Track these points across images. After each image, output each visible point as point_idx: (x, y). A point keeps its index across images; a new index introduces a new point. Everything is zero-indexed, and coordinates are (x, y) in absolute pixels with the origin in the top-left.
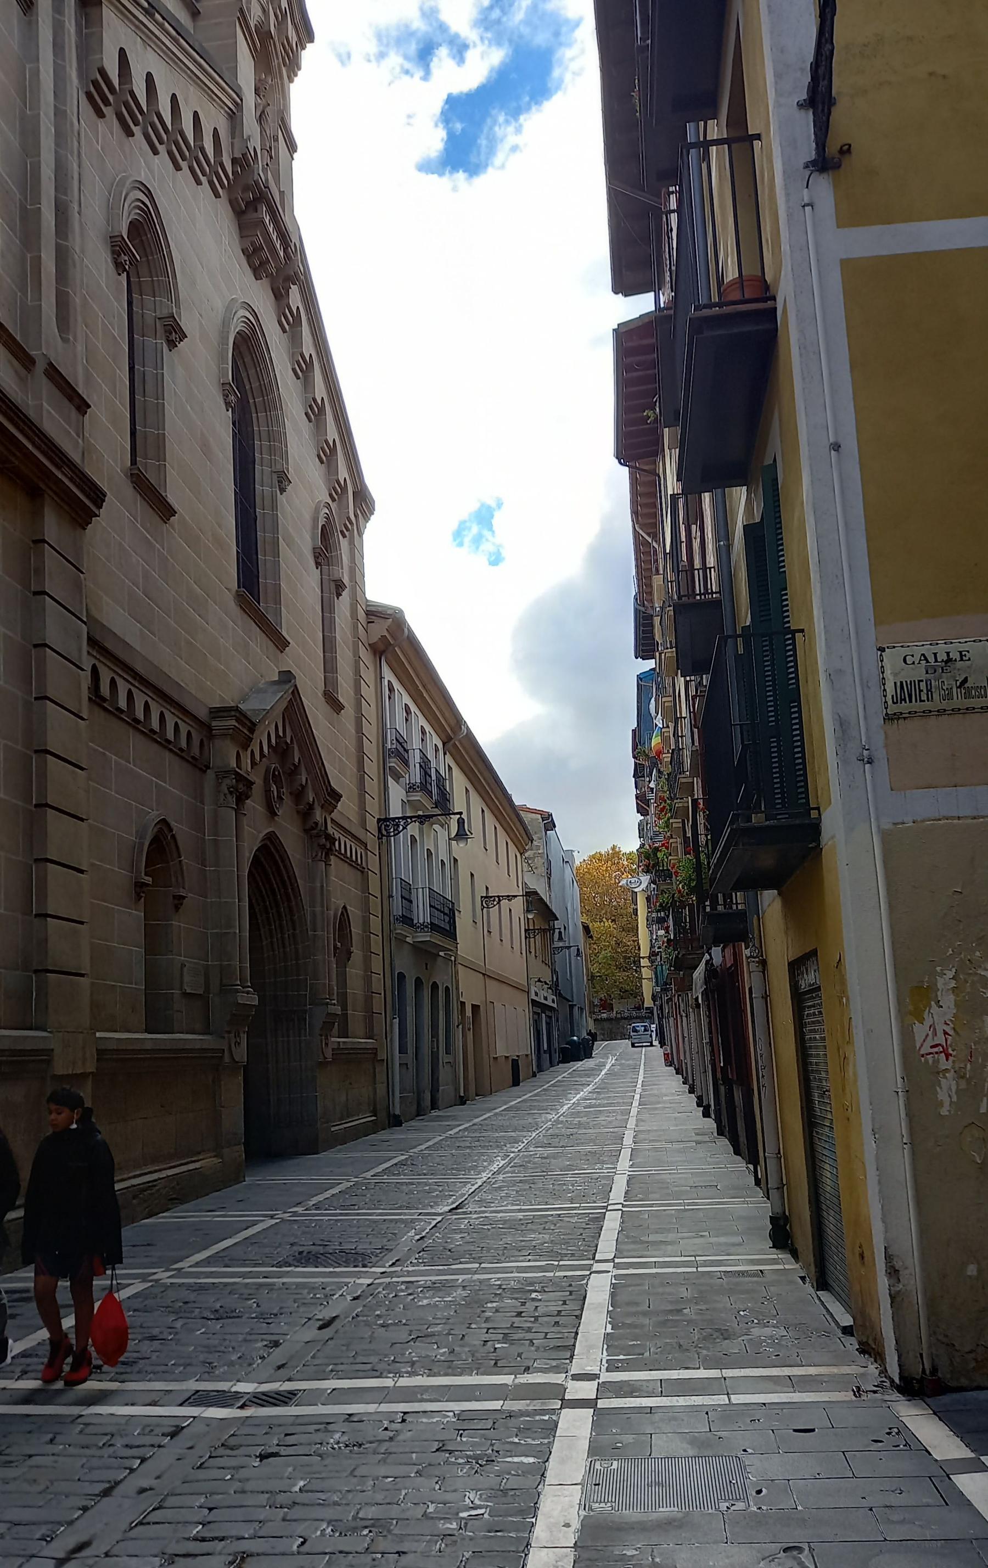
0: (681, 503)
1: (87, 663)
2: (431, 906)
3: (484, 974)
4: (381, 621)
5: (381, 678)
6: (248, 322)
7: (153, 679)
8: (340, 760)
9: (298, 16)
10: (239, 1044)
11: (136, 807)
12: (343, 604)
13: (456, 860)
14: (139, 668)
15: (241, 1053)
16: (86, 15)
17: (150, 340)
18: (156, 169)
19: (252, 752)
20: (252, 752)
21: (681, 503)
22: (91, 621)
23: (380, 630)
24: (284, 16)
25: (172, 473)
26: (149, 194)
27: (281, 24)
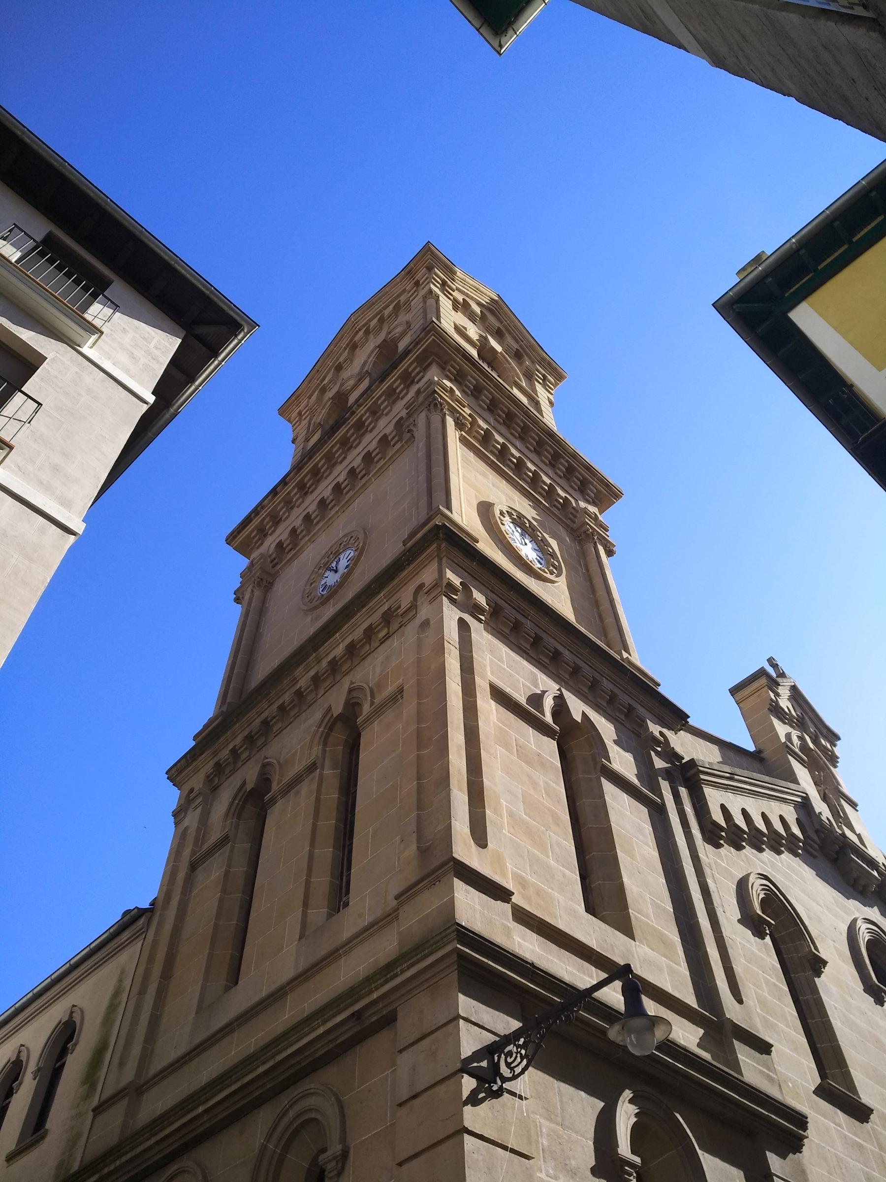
6: (871, 931)
9: (825, 731)
26: (766, 878)
27: (815, 741)
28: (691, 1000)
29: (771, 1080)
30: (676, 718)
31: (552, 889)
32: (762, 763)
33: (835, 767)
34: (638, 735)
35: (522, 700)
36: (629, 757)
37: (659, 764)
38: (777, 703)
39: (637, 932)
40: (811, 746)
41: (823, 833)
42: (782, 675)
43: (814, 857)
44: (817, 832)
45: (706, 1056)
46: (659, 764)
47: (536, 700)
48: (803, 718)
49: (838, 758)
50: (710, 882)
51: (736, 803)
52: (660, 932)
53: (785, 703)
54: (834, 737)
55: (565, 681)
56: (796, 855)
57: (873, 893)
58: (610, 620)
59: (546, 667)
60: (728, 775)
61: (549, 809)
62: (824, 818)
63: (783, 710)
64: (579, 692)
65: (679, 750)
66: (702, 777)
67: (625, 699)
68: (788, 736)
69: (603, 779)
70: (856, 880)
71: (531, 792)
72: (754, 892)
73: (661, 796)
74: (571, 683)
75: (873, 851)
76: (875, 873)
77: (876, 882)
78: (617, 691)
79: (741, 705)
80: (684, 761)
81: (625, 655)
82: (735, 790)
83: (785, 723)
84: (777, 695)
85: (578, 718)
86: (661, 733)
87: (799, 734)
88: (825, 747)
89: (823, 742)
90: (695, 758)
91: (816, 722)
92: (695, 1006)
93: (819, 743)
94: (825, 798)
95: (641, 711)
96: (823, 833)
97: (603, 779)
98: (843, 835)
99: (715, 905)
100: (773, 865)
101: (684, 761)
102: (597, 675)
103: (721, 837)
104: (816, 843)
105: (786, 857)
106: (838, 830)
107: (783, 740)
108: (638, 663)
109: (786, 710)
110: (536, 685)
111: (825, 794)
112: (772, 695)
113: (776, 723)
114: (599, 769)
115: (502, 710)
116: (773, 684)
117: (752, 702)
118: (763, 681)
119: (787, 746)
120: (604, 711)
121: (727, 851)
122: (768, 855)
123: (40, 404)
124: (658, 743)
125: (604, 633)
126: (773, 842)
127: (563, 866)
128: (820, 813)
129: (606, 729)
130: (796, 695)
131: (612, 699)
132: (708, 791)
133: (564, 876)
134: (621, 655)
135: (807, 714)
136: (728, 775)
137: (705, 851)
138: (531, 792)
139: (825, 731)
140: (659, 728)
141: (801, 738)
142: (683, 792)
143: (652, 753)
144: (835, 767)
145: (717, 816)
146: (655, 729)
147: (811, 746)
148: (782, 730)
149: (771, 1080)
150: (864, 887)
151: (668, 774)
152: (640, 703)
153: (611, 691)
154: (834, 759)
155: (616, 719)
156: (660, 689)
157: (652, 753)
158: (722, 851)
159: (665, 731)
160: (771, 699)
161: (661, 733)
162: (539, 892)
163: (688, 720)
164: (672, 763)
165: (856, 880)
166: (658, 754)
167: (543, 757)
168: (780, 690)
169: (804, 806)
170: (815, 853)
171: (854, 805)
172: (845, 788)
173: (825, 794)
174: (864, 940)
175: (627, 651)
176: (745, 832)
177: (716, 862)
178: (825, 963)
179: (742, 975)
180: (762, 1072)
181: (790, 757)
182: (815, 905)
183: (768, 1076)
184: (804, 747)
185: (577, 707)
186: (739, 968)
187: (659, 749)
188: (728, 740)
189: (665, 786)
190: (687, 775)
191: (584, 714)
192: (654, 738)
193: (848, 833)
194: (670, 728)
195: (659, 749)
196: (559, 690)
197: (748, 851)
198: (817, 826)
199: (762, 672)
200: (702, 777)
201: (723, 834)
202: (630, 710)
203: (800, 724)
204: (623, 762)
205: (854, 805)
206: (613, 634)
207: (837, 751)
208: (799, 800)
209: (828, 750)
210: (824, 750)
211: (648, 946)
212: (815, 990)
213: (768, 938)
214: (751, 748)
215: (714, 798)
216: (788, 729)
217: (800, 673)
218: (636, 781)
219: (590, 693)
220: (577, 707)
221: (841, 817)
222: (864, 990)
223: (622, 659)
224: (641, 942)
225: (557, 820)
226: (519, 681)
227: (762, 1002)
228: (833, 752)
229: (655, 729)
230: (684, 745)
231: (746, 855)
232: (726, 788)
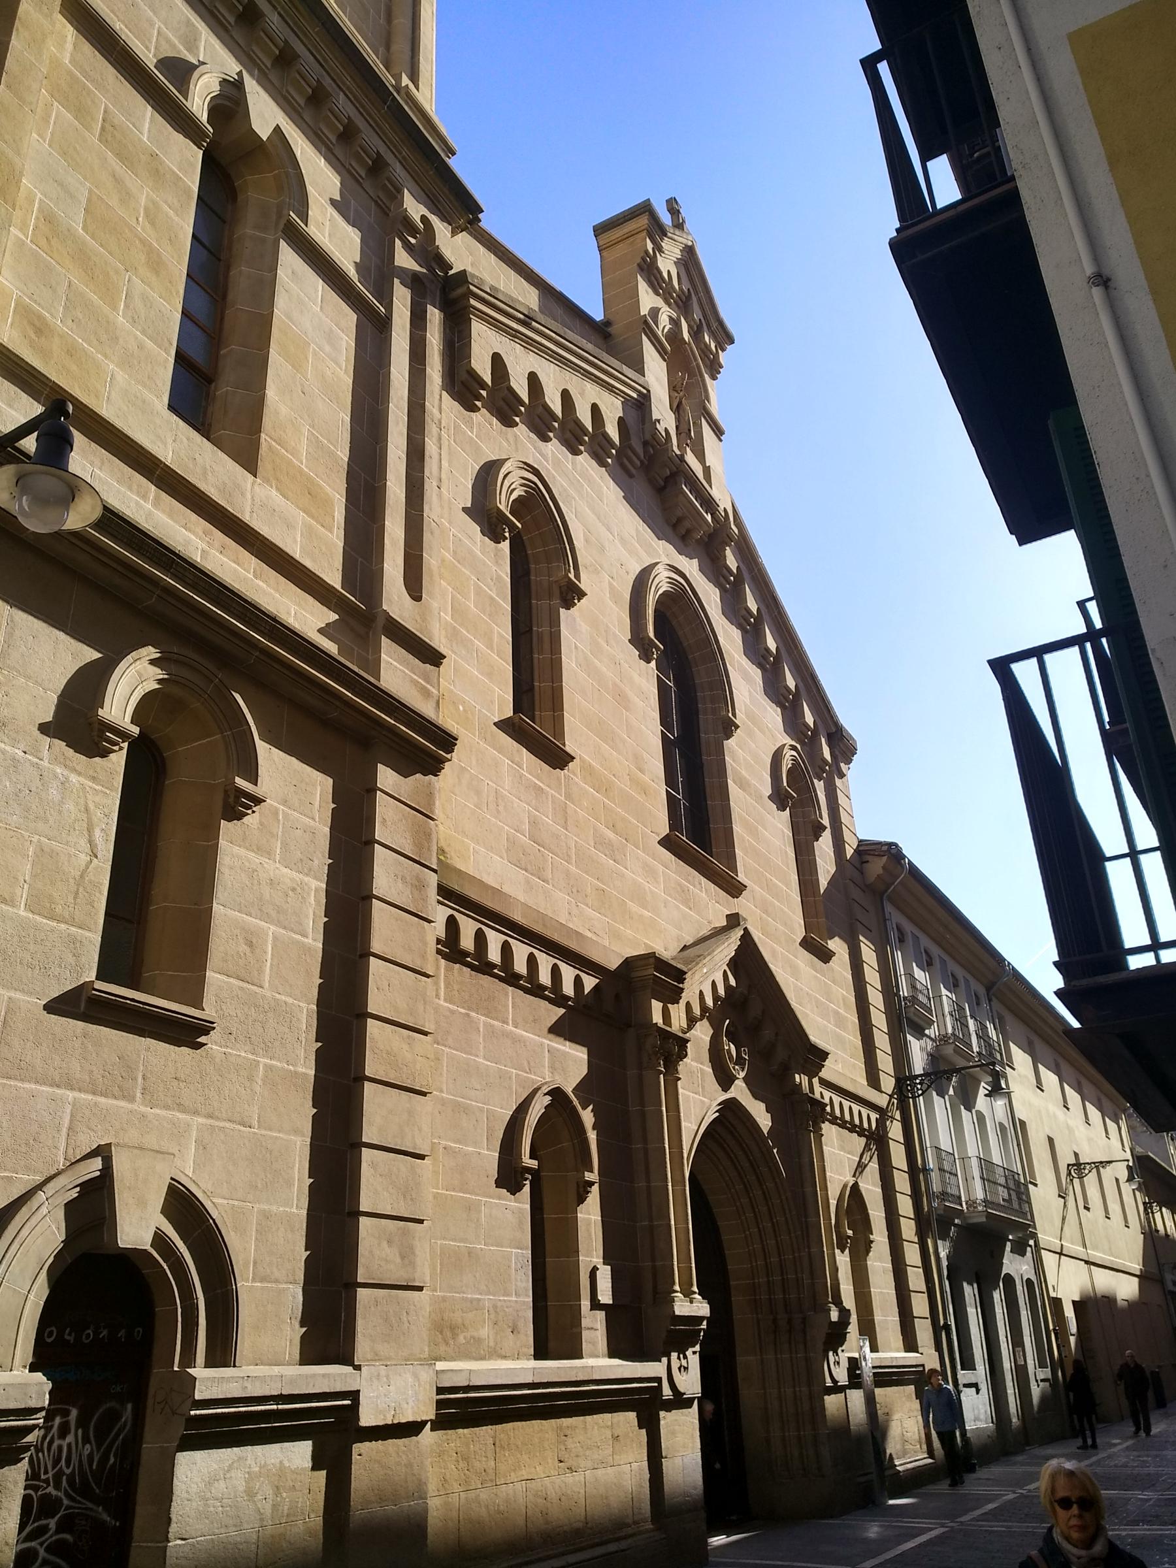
0: (883, 68)
1: (441, 914)
2: (956, 1175)
3: (1087, 1262)
4: (876, 859)
5: (885, 920)
6: (672, 581)
7: (538, 928)
8: (837, 1013)
9: (715, 325)
10: (686, 1369)
11: (517, 1075)
12: (824, 846)
13: (1023, 1123)
14: (517, 917)
15: (690, 1382)
16: (459, 332)
17: (544, 603)
18: (551, 456)
19: (688, 1005)
20: (688, 1005)
21: (883, 68)
22: (443, 868)
23: (876, 867)
24: (700, 327)
25: (571, 720)
26: (536, 472)
27: (696, 333)
28: (334, 579)
29: (426, 694)
30: (462, 208)
31: (106, 356)
32: (608, 339)
33: (714, 378)
34: (384, 211)
35: (149, 59)
36: (353, 236)
37: (403, 259)
38: (654, 259)
39: (264, 464)
40: (686, 336)
41: (653, 447)
42: (679, 225)
43: (631, 476)
44: (645, 444)
45: (331, 647)
46: (403, 259)
47: (181, 71)
48: (689, 297)
49: (721, 367)
50: (431, 446)
51: (521, 364)
52: (309, 478)
53: (667, 265)
54: (725, 338)
55: (260, 69)
56: (602, 463)
57: (697, 541)
58: (401, 21)
59: (226, 30)
60: (522, 316)
61: (143, 242)
62: (661, 428)
63: (660, 273)
64: (285, 98)
65: (447, 253)
66: (472, 302)
67: (372, 140)
68: (655, 312)
69: (283, 244)
70: (679, 520)
71: (114, 202)
72: (507, 483)
73: (389, 307)
74: (272, 77)
75: (716, 492)
76: (709, 518)
77: (706, 528)
78: (360, 122)
79: (605, 253)
80: (451, 272)
81: (405, 81)
82: (529, 343)
83: (658, 294)
84: (659, 248)
85: (264, 133)
86: (424, 219)
87: (674, 315)
88: (708, 347)
89: (707, 338)
90: (469, 269)
91: (707, 308)
92: (338, 586)
93: (700, 340)
94: (677, 409)
95: (398, 171)
96: (653, 447)
97: (283, 244)
98: (681, 458)
99: (427, 473)
100: (557, 463)
101: (451, 272)
102: (327, 82)
103: (479, 397)
104: (638, 458)
105: (585, 460)
106: (675, 449)
107: (644, 311)
108: (430, 108)
109: (665, 275)
110: (192, 45)
111: (680, 404)
112: (650, 246)
113: (643, 287)
114: (281, 226)
115: (87, 48)
116: (657, 231)
117: (621, 250)
118: (643, 221)
119: (646, 322)
120: (329, 149)
121: (483, 418)
122: (554, 448)
123: (1002, 667)
124: (414, 231)
125: (386, 43)
126: (568, 435)
127: (143, 332)
128: (659, 421)
129: (321, 177)
130: (689, 260)
131: (348, 135)
132: (479, 330)
133: (141, 347)
134: (398, 78)
135: (697, 293)
136: (522, 316)
137: (442, 407)
138: (114, 202)
139: (715, 325)
140: (424, 211)
141: (675, 322)
142: (434, 315)
143: (398, 243)
144: (714, 378)
145: (482, 366)
146: (415, 209)
147: (686, 336)
148: (648, 300)
149: (426, 694)
150: (688, 532)
151: (414, 282)
152: (400, 160)
153: (349, 118)
154: (714, 368)
155: (349, 172)
156: (453, 162)
157: (398, 243)
158: (475, 416)
159: (434, 220)
160: (647, 252)
161: (424, 219)
162: (72, 351)
163: (480, 216)
164: (431, 269)
165: (679, 520)
166: (408, 247)
167: (162, 163)
168: (666, 244)
169: (640, 405)
170: (633, 471)
171: (718, 432)
172: (714, 407)
173: (680, 404)
174: (657, 590)
175: (414, 77)
176: (522, 403)
177: (456, 427)
178: (581, 594)
179: (435, 569)
180: (416, 683)
181: (644, 337)
182: (603, 530)
183: (424, 688)
184: (674, 335)
185: (265, 114)
186: (431, 560)
187: (413, 241)
188: (559, 286)
189: (402, 297)
190: (450, 294)
191: (277, 129)
192: (407, 222)
193: (690, 458)
194: (444, 218)
195: (413, 241)
196: (240, 74)
197: (521, 431)
198: (648, 437)
199: (645, 209)
200: (472, 302)
201: (484, 393)
202: (377, 167)
203: (682, 304)
204: (343, 242)
205: (718, 432)
206: (400, 46)
207: (723, 357)
208: (635, 395)
209: (711, 352)
210: (705, 350)
211: (278, 489)
212: (555, 622)
213: (505, 546)
214: (598, 315)
215: (484, 342)
216: (659, 302)
217: (701, 231)
218: (352, 272)
219: (308, 106)
220: (265, 114)
221: (690, 438)
222: (172, 407)
223: (398, 88)
224: (267, 481)
225: (156, 264)
226: (152, 25)
227: (458, 611)
228: (716, 356)
229: (415, 209)
230: (459, 251)
231: (516, 436)
232: (514, 335)
